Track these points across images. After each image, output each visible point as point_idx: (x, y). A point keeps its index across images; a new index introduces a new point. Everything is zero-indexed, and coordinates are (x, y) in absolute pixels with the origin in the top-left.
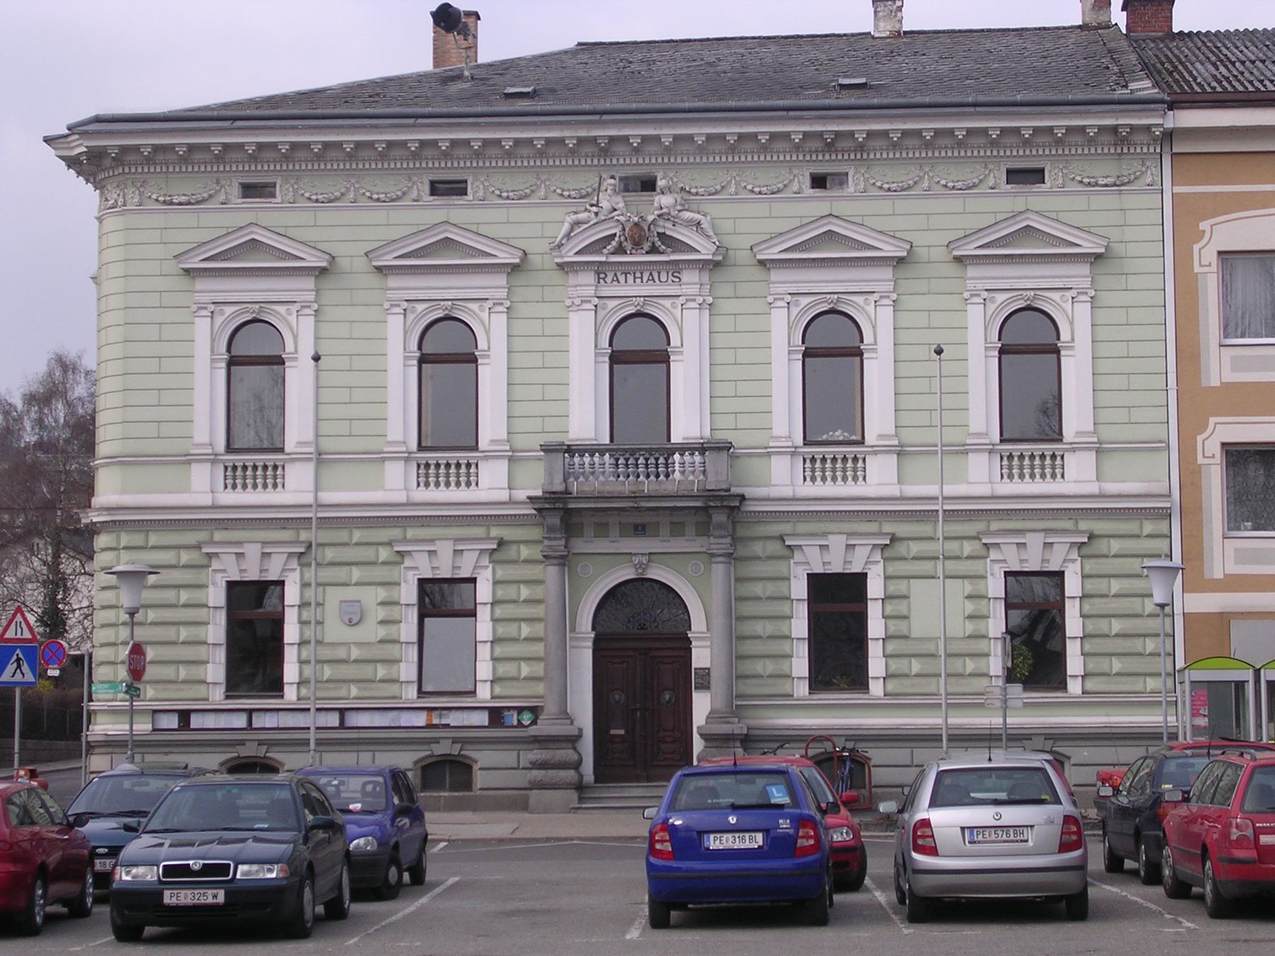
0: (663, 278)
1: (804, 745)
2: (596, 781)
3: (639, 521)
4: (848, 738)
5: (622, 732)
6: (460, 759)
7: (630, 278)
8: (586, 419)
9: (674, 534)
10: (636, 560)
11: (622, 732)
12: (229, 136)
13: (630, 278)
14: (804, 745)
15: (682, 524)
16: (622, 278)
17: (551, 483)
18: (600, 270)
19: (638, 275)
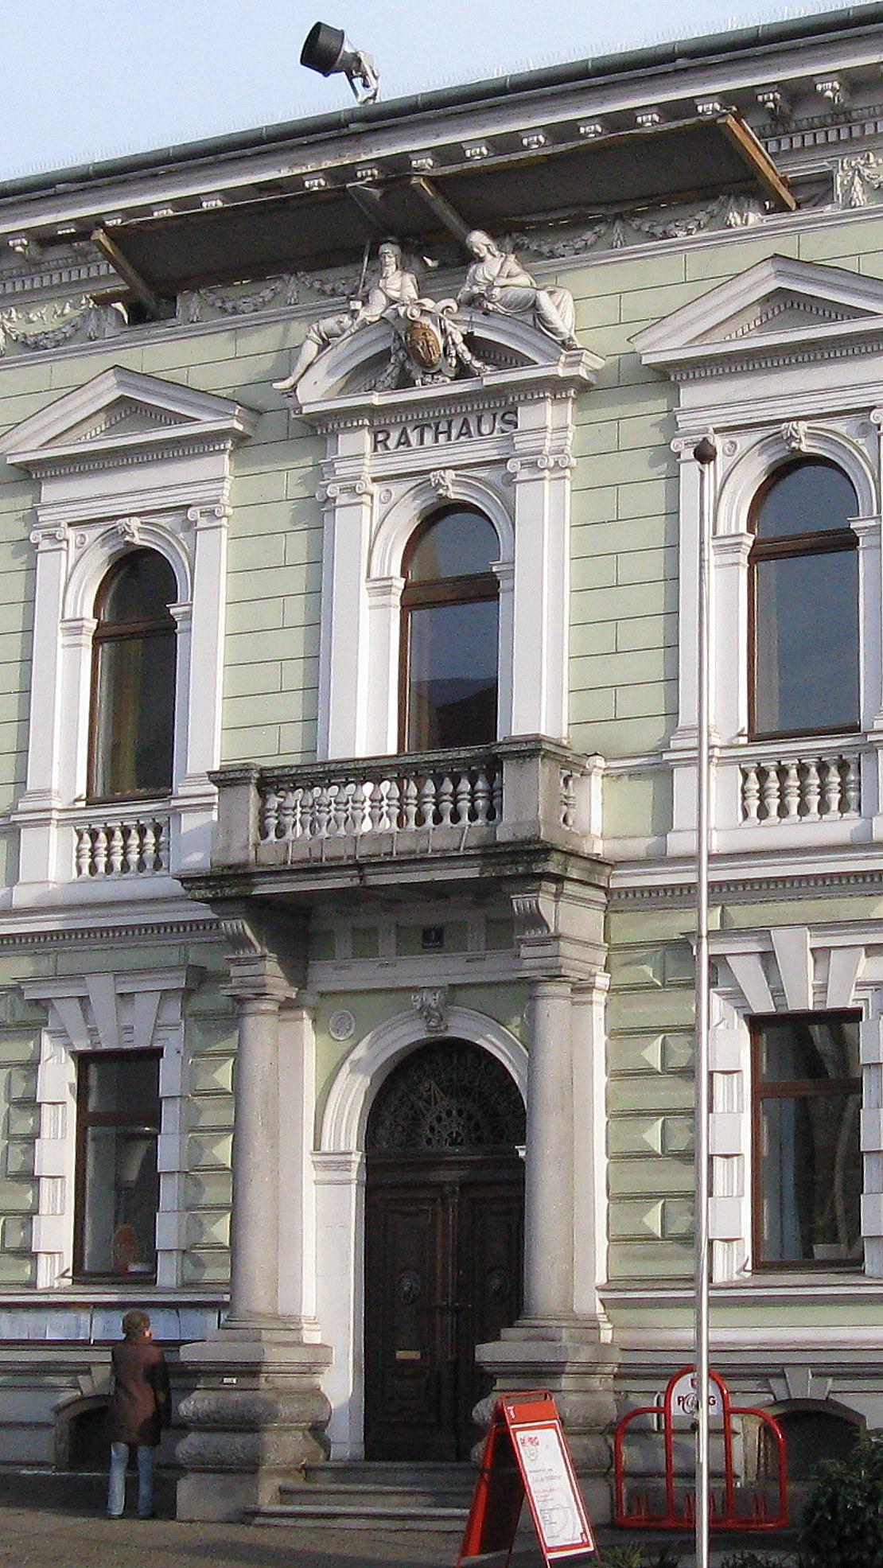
0: (485, 429)
1: (663, 1385)
2: (370, 1455)
3: (433, 920)
4: (821, 1371)
5: (414, 1355)
6: (829, 1410)
7: (429, 437)
8: (368, 718)
9: (358, 954)
10: (416, 1000)
11: (414, 1355)
12: (518, 117)
13: (429, 437)
14: (663, 1385)
15: (374, 931)
16: (413, 437)
17: (227, 849)
18: (379, 420)
19: (443, 427)
